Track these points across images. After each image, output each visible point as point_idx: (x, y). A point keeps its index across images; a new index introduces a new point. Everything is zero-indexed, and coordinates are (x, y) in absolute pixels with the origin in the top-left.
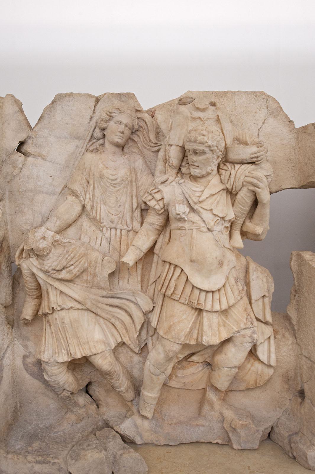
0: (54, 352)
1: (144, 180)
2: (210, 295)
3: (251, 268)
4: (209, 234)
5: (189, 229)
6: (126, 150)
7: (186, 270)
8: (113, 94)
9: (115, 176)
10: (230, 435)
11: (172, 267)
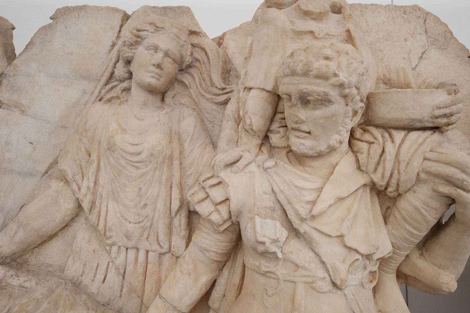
1: (197, 154)
4: (336, 298)
5: (285, 281)
6: (168, 100)
8: (154, 7)
9: (139, 146)
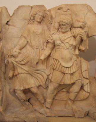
0: (19, 86)
2: (67, 69)
3: (82, 61)
4: (67, 50)
6: (41, 23)
7: (60, 61)
10: (75, 113)
11: (56, 60)
